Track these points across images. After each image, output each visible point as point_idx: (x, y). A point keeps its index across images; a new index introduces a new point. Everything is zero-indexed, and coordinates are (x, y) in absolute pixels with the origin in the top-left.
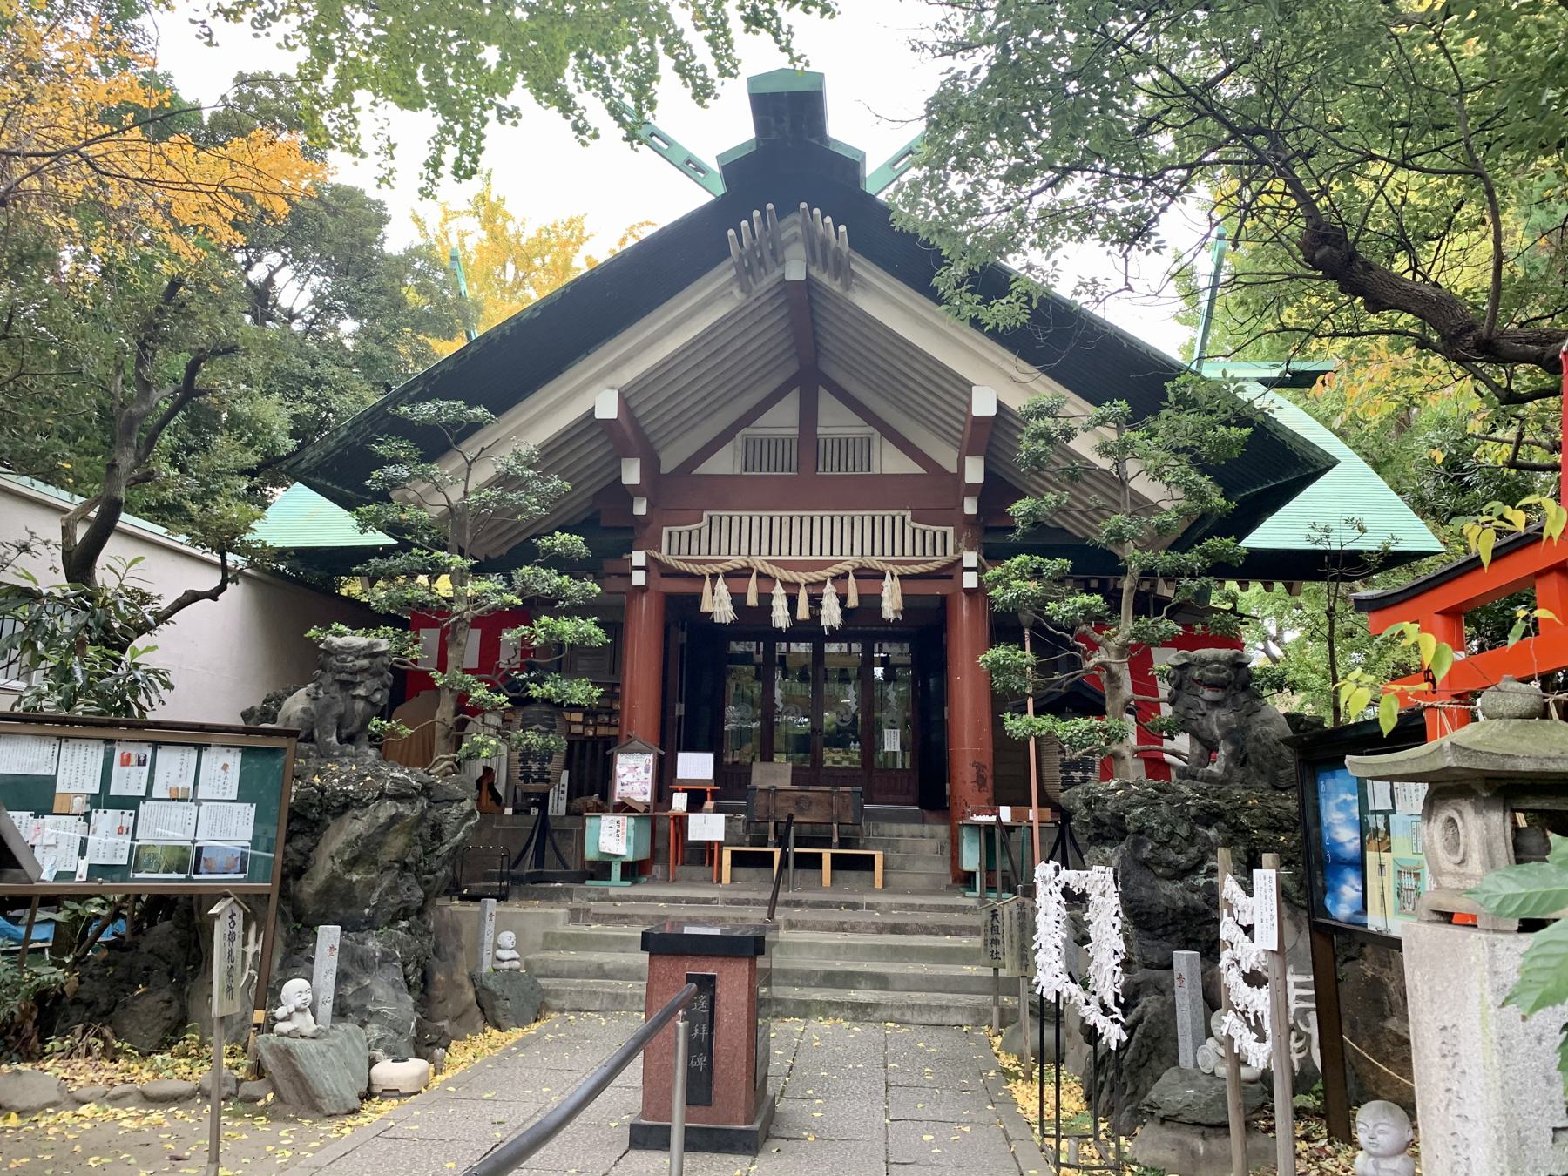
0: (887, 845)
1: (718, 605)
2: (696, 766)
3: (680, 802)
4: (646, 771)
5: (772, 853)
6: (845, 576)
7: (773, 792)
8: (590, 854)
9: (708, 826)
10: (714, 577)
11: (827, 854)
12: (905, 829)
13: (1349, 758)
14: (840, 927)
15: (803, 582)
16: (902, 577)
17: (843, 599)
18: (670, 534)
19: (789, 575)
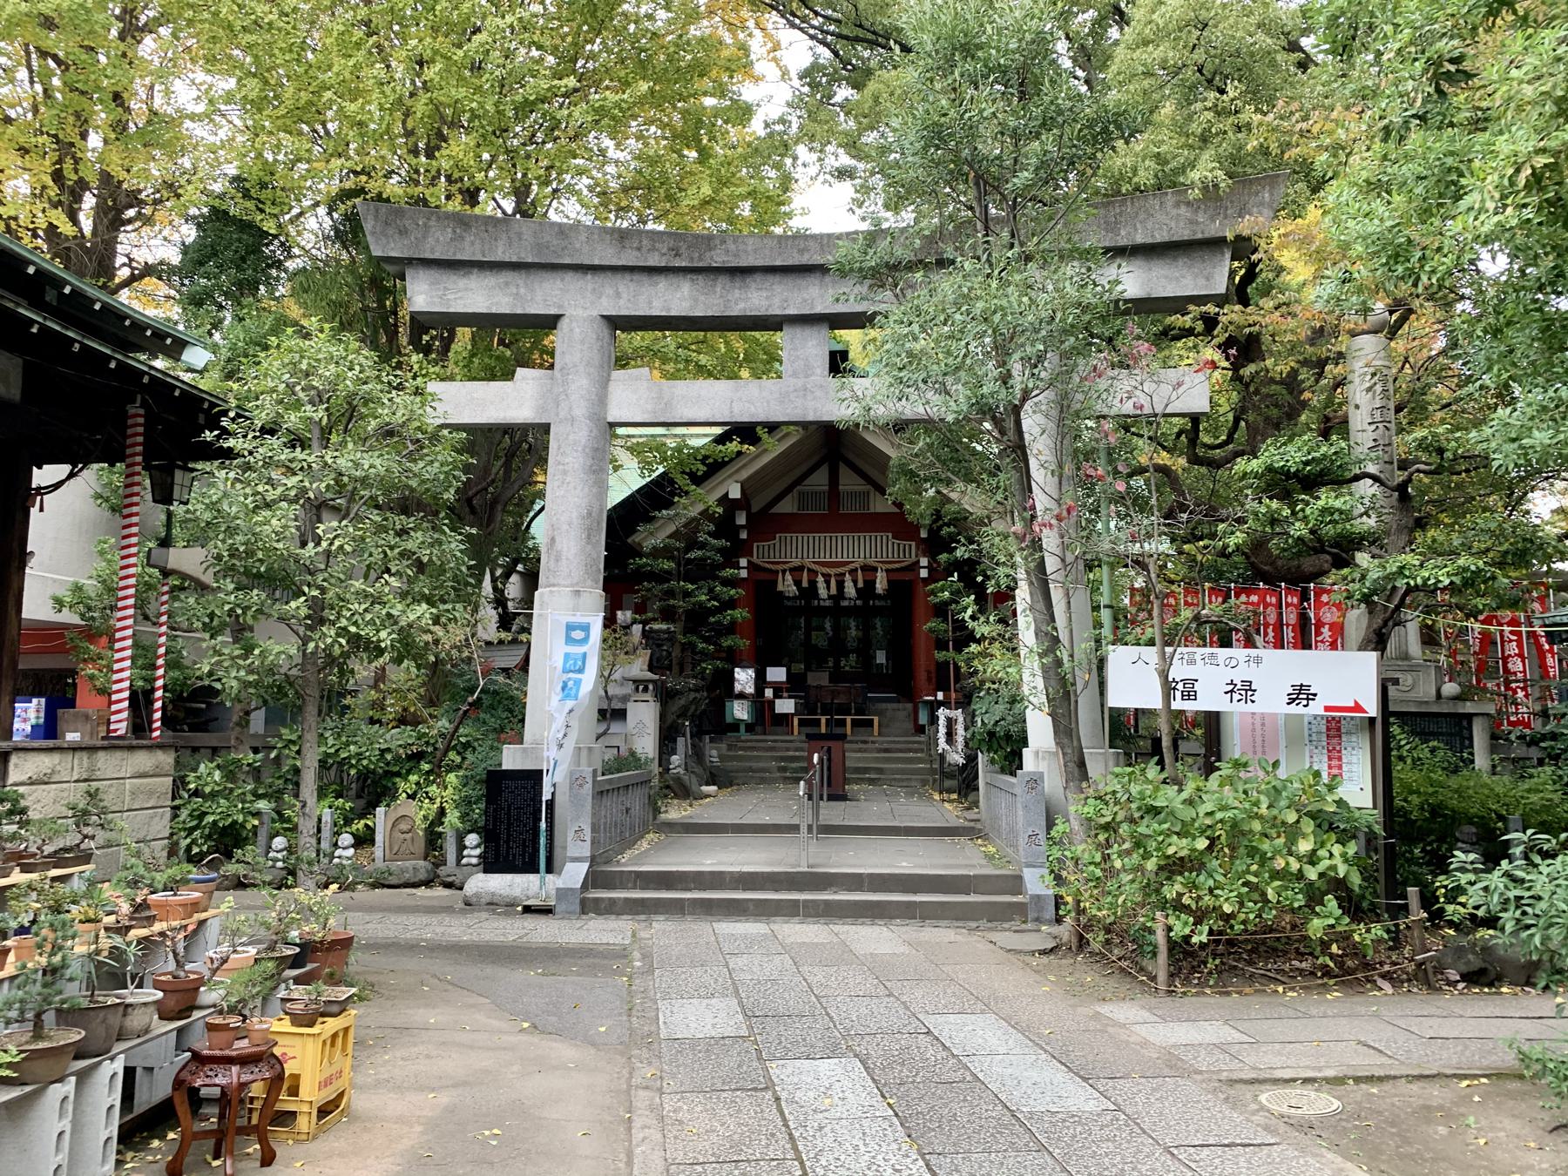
0: (880, 713)
1: (787, 585)
2: (777, 674)
3: (769, 693)
6: (856, 570)
7: (820, 687)
8: (729, 720)
9: (785, 706)
10: (784, 572)
11: (849, 719)
12: (890, 706)
14: (860, 750)
16: (887, 571)
17: (855, 582)
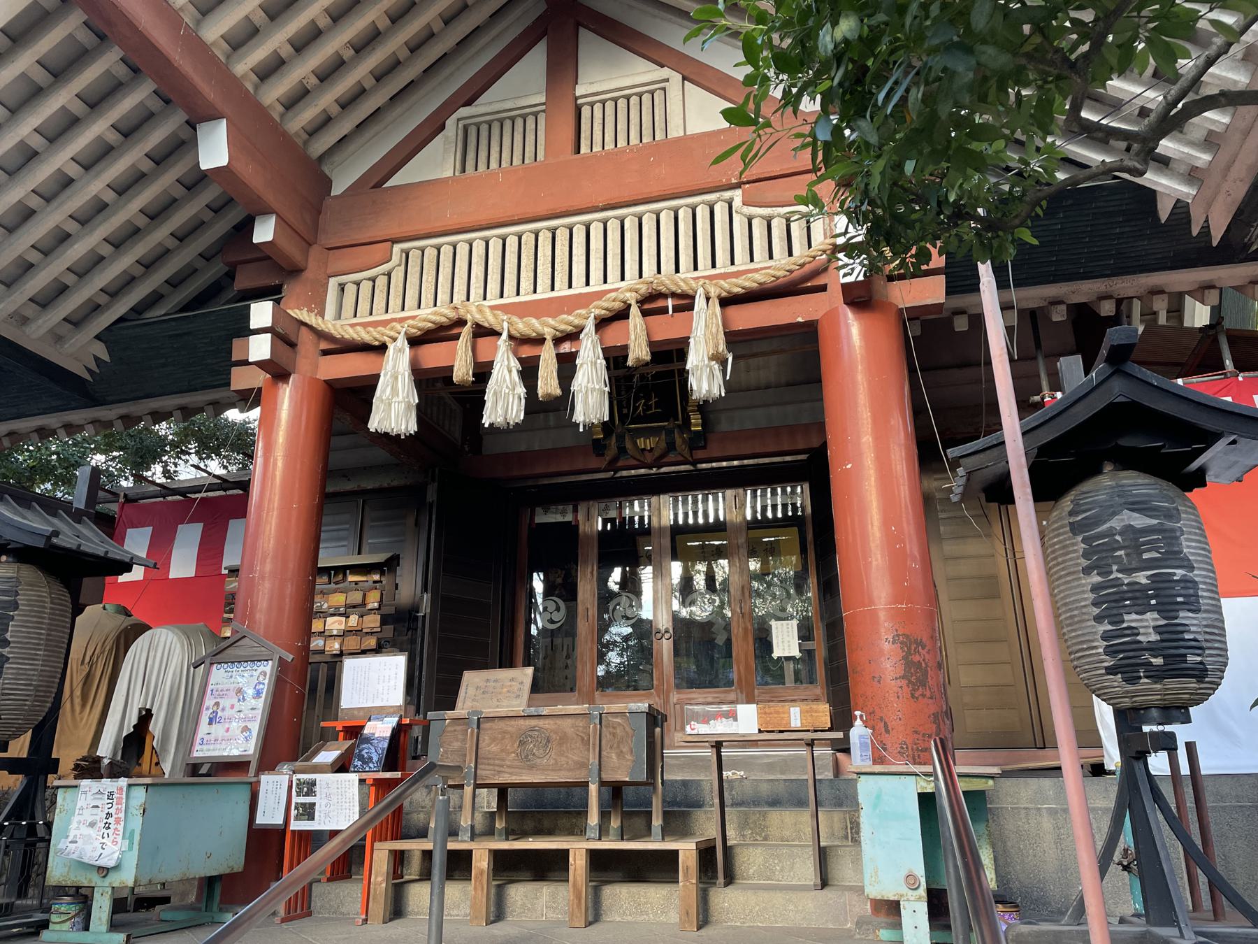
4: (258, 694)
5: (468, 854)
13: (53, 756)
15: (548, 333)
17: (615, 359)
18: (342, 287)
19: (524, 326)
